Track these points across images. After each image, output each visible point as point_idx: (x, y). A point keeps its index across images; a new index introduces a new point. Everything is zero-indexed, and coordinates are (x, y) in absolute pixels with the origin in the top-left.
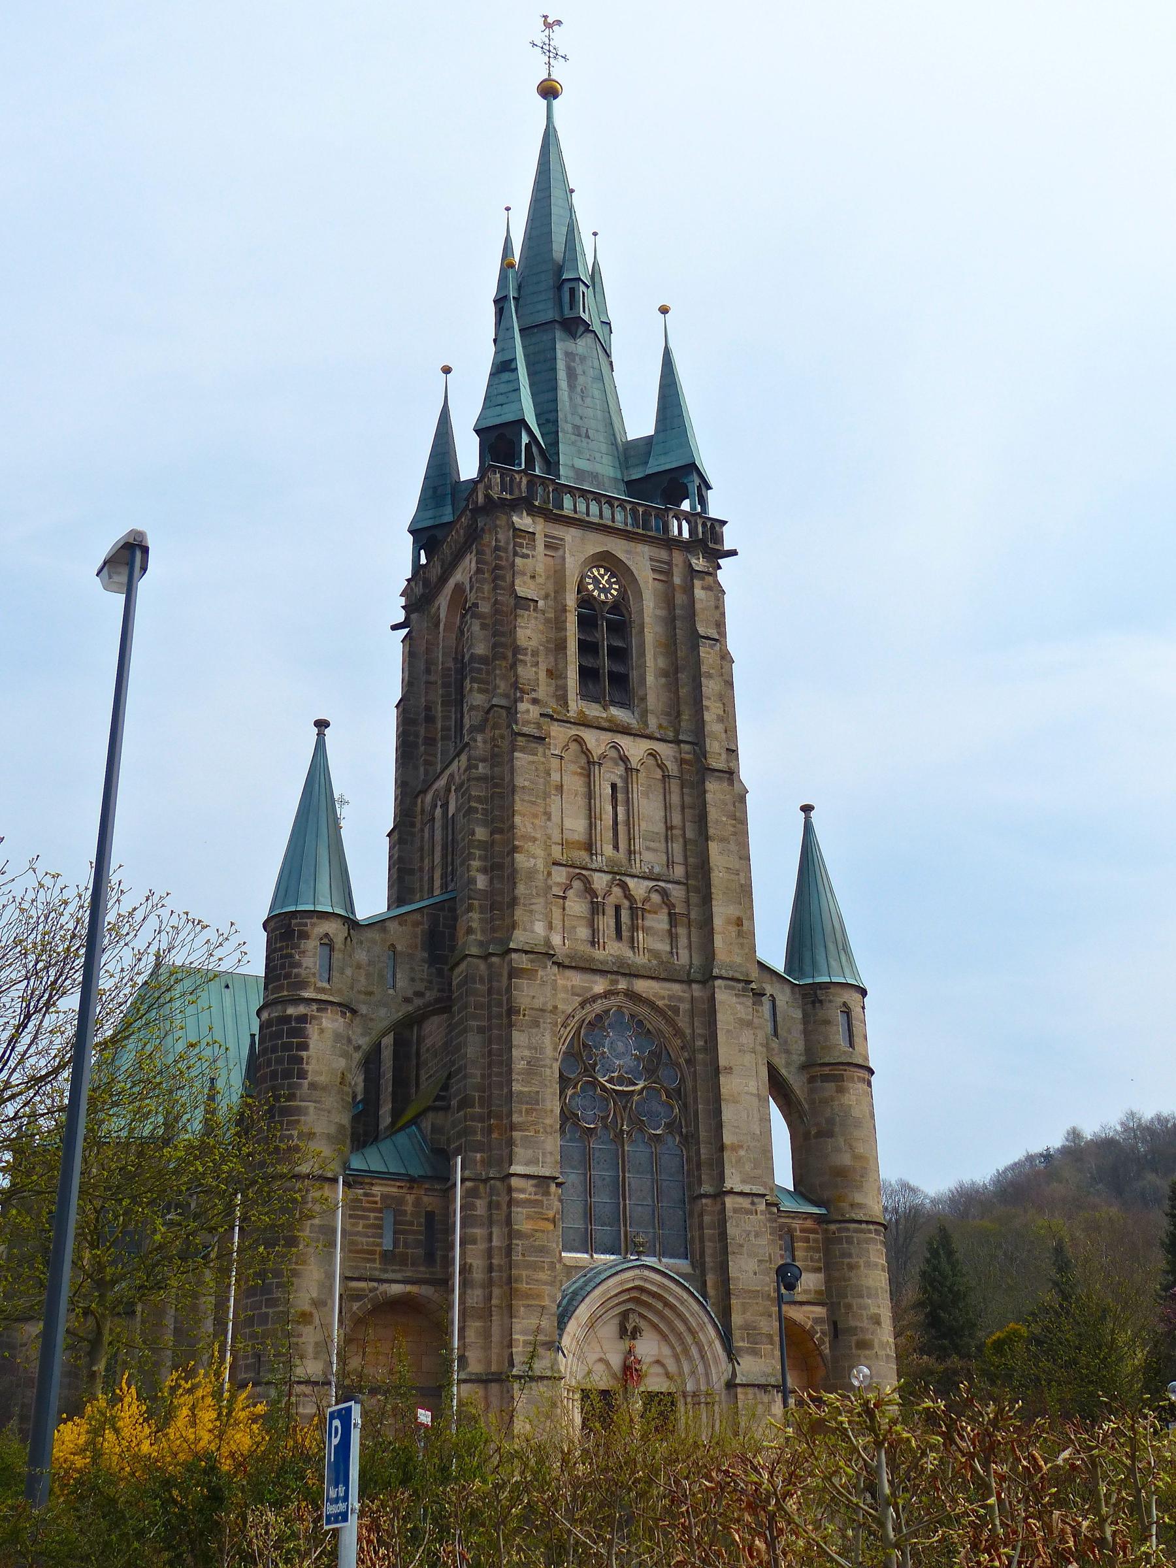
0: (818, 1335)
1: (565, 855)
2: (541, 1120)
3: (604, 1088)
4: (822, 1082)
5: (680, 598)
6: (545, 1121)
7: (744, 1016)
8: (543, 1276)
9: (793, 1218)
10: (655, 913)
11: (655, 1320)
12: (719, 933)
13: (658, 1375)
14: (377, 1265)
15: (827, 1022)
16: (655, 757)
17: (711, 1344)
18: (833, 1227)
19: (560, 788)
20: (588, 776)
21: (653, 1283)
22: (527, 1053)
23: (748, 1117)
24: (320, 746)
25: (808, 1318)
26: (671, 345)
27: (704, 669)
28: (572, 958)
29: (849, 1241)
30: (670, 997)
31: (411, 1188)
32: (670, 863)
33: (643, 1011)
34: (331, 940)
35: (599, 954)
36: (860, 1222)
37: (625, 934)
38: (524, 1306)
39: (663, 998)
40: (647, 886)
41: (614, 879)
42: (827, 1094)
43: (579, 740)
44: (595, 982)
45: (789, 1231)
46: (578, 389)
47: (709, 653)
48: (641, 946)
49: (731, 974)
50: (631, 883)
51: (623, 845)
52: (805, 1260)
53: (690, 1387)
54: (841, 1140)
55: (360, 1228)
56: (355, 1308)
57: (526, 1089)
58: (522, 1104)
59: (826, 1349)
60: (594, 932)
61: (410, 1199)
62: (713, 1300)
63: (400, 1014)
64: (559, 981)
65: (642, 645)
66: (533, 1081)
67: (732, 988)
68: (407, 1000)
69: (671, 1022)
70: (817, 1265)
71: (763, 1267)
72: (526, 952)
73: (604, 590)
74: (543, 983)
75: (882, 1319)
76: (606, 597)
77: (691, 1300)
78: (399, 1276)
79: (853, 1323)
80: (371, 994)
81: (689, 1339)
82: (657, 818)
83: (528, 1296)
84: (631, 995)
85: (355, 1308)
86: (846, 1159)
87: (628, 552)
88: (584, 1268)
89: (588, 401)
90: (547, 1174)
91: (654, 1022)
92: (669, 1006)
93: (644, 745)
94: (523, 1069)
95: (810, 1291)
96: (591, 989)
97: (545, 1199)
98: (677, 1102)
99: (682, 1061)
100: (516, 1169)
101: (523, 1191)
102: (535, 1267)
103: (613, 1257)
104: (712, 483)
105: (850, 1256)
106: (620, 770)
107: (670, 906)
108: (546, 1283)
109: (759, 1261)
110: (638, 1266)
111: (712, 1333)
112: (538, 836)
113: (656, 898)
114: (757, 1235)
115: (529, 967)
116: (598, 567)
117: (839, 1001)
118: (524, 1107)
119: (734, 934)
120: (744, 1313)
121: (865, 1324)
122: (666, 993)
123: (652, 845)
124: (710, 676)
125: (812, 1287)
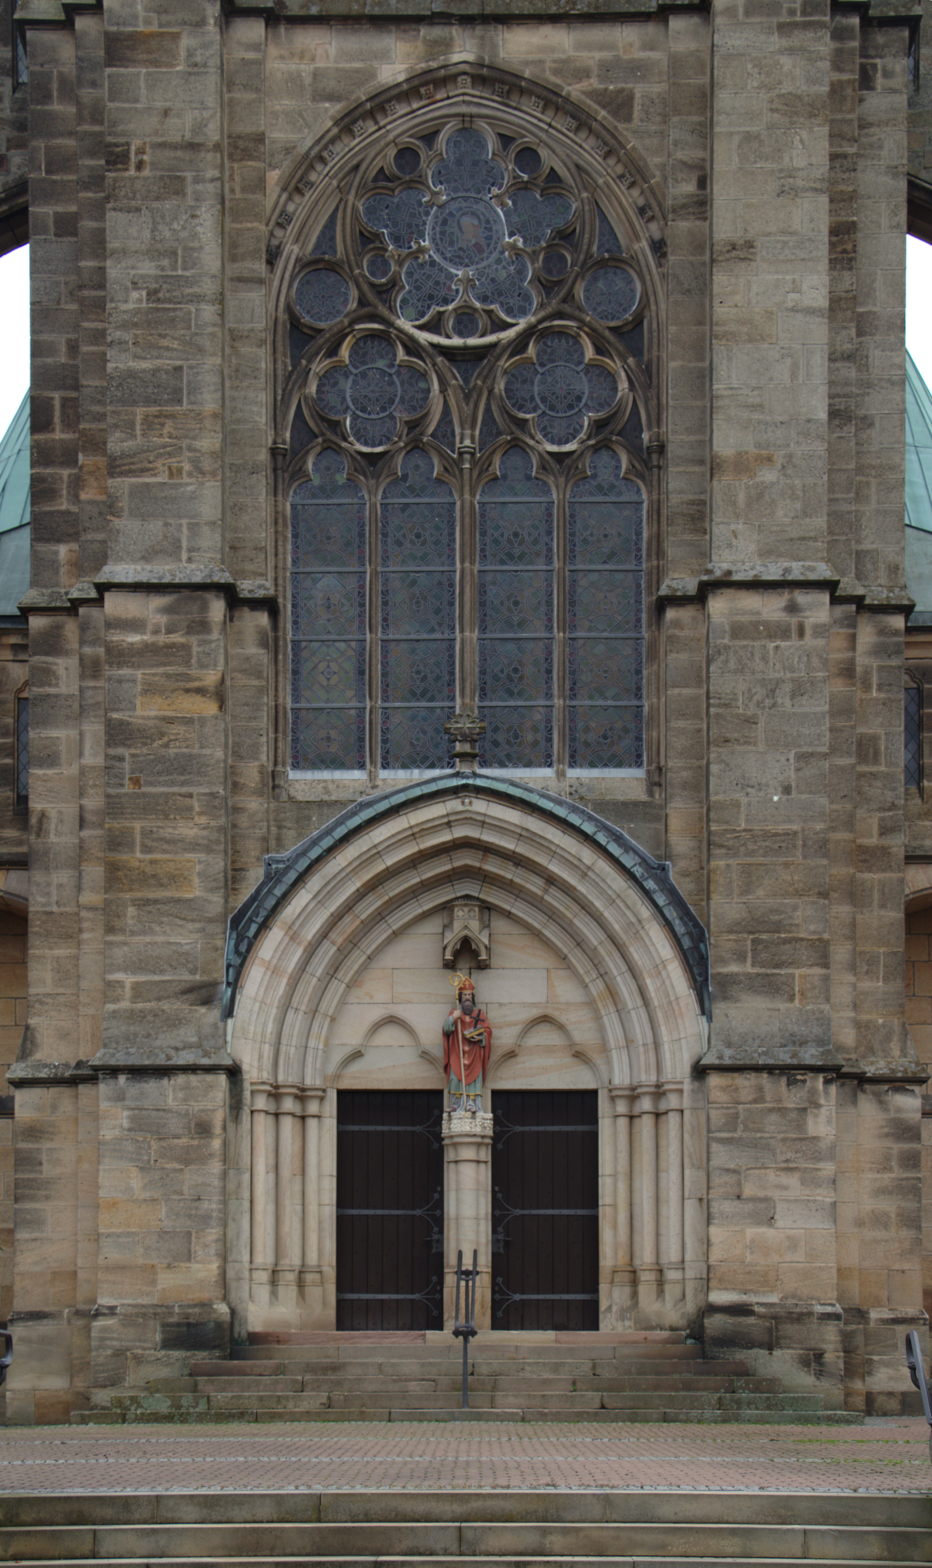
2: (185, 443)
3: (413, 347)
6: (197, 444)
7: (802, 88)
13: (549, 1050)
17: (659, 968)
21: (500, 828)
22: (147, 268)
23: (794, 376)
30: (607, 69)
38: (134, 902)
57: (145, 365)
58: (134, 403)
62: (682, 864)
66: (165, 342)
77: (603, 866)
81: (614, 964)
83: (146, 879)
90: (197, 578)
92: (601, 97)
94: (137, 311)
96: (371, 75)
97: (193, 640)
98: (624, 361)
109: (801, 757)
114: (796, 693)
115: (154, 28)
118: (140, 412)
120: (746, 890)
122: (592, 58)
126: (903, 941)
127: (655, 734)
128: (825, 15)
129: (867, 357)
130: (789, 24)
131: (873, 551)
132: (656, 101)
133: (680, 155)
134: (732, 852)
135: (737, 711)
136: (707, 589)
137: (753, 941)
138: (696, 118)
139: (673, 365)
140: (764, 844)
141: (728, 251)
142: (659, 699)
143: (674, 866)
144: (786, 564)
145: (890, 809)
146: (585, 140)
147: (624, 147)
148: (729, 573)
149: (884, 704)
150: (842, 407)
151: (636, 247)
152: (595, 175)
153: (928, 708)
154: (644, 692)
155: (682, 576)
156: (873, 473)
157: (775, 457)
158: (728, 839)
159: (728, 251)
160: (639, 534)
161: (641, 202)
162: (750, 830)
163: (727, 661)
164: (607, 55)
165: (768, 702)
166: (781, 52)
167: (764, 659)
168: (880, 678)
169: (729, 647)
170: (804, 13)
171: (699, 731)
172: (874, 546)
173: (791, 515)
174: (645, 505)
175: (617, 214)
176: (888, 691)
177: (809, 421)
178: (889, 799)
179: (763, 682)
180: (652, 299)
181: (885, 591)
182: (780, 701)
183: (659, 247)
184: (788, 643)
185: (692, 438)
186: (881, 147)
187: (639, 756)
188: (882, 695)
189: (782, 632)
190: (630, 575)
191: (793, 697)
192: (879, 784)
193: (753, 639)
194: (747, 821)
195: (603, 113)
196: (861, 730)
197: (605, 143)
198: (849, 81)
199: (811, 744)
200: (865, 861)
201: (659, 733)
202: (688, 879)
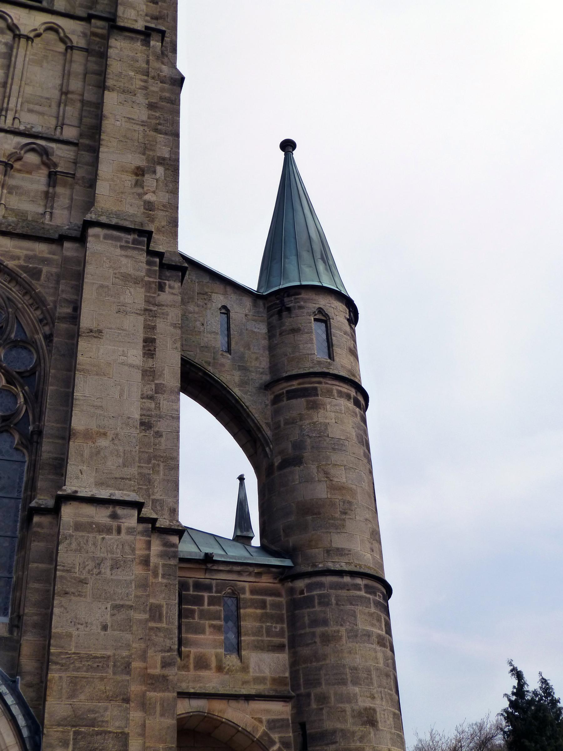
4: (289, 399)
9: (239, 573)
10: (29, 172)
16: (57, 31)
18: (301, 584)
23: (121, 395)
25: (260, 721)
29: (324, 601)
30: (28, 258)
36: (340, 573)
39: (18, 258)
40: (18, 143)
42: (294, 414)
45: (233, 593)
49: (114, 221)
52: (258, 632)
54: (313, 468)
62: (28, 678)
67: (118, 239)
69: (27, 290)
70: (277, 640)
71: (121, 616)
75: (379, 716)
79: (328, 725)
92: (25, 269)
98: (22, 388)
99: (40, 337)
105: (325, 623)
109: (115, 607)
114: (115, 566)
117: (313, 307)
119: (128, 184)
120: (72, 695)
121: (350, 725)
123: (37, 108)
126: (176, 739)
127: (18, 594)
128: (144, 246)
129: (159, 403)
130: (126, 246)
131: (161, 500)
132: (54, 275)
133: (64, 296)
134: (64, 667)
135: (74, 575)
136: (62, 500)
137: (75, 732)
138: (73, 282)
139: (51, 388)
140: (87, 663)
141: (88, 333)
142: (23, 573)
143: (22, 679)
144: (113, 491)
145: (168, 651)
146: (14, 287)
147: (34, 291)
148: (76, 492)
149: (166, 586)
150: (147, 421)
151: (36, 336)
152: (17, 303)
153: (184, 605)
154: (14, 569)
155: (46, 498)
156: (162, 459)
157: (108, 434)
158: (62, 659)
159: (88, 333)
160: (21, 479)
161: (41, 317)
162: (78, 653)
163: (71, 544)
164: (31, 253)
165: (95, 571)
166: (121, 256)
167: (94, 544)
168: (163, 570)
169: (73, 536)
170: (133, 243)
171: (48, 591)
172: (162, 497)
173: (116, 465)
174: (26, 464)
175: (27, 321)
176: (168, 579)
177: (129, 418)
178: (168, 645)
179: (93, 559)
180: (42, 361)
181: (168, 521)
182: (103, 570)
183: (49, 338)
184: (110, 537)
185: (59, 425)
186: (168, 315)
187: (6, 609)
188: (165, 581)
189: (109, 530)
190: (13, 501)
191: (112, 569)
192: (162, 635)
193: (89, 532)
194: (76, 647)
195: (25, 275)
196: (152, 600)
197: (24, 288)
198: (153, 282)
199: (122, 599)
200: (152, 684)
201: (21, 593)
202: (31, 689)
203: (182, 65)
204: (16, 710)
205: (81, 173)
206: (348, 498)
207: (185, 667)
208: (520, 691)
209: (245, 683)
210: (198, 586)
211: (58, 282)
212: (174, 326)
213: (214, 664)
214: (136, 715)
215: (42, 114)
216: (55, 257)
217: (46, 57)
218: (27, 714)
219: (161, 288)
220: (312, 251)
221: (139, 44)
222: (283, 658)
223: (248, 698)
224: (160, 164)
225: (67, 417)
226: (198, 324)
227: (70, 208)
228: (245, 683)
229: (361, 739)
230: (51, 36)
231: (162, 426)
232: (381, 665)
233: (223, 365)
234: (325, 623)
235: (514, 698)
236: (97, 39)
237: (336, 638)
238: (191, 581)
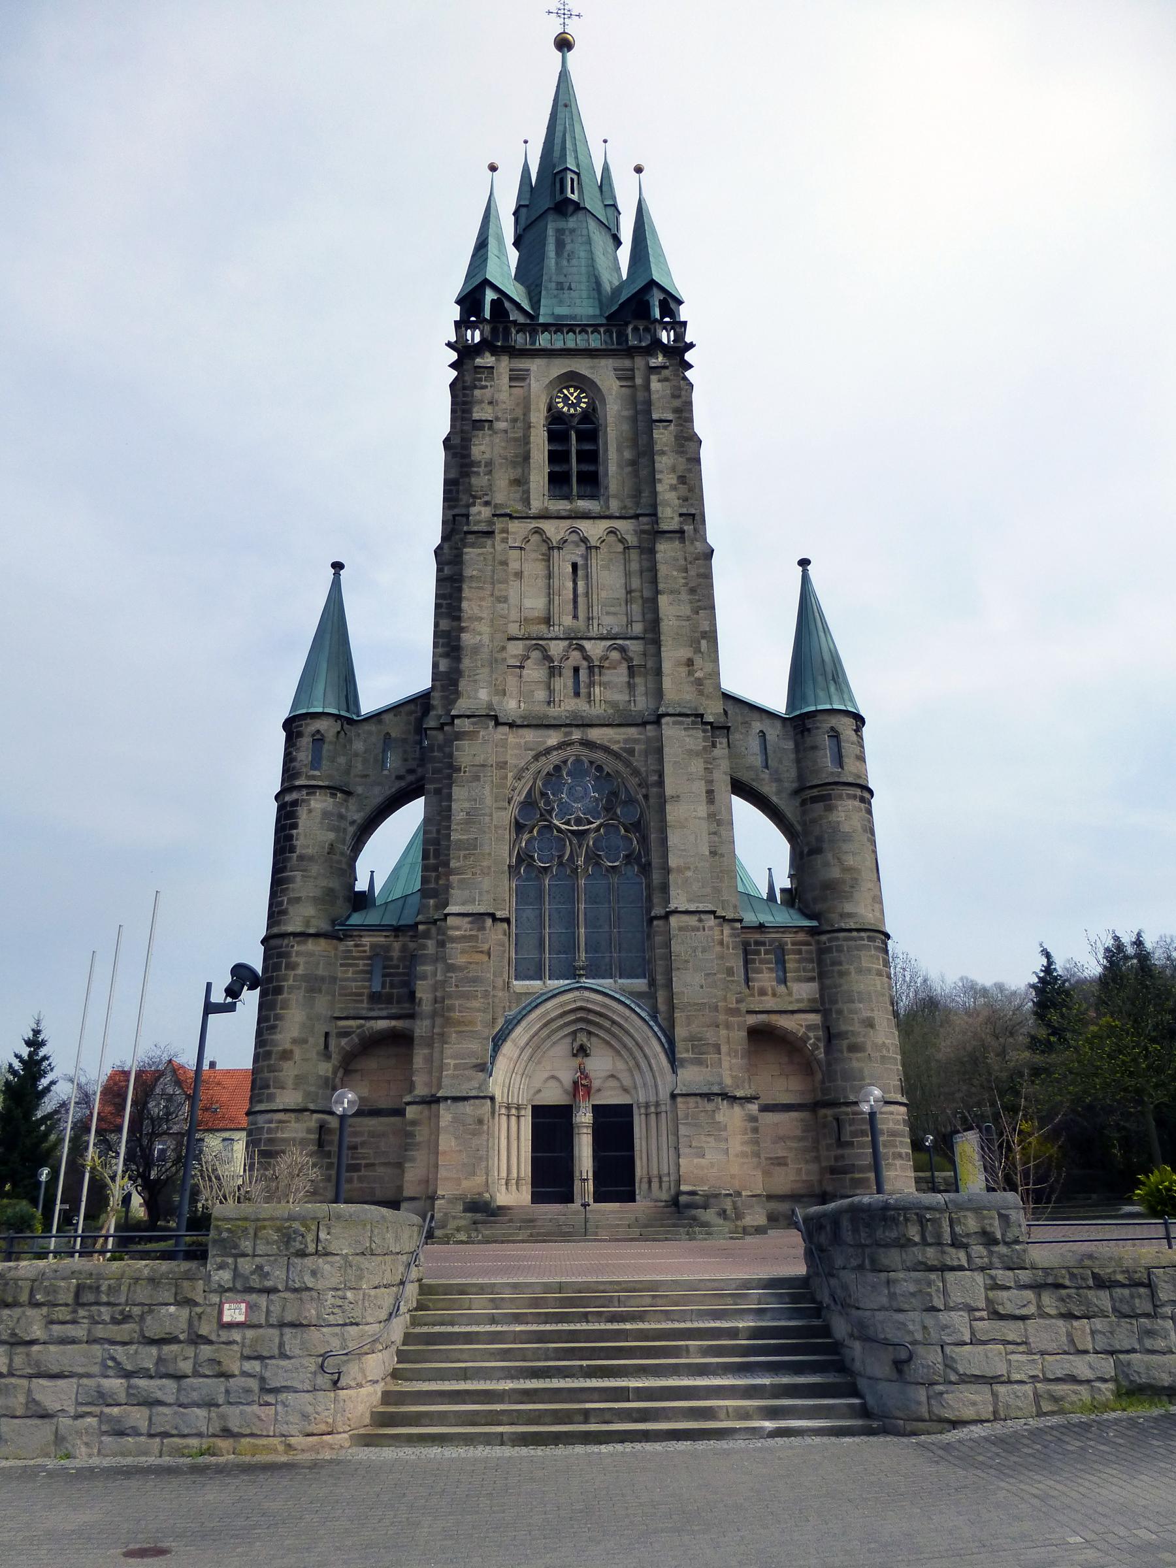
0: (811, 1041)
1: (523, 631)
3: (559, 830)
5: (641, 396)
8: (475, 1004)
9: (783, 932)
10: (615, 668)
11: (607, 1037)
12: (668, 675)
14: (365, 1005)
15: (814, 748)
18: (824, 938)
19: (519, 575)
20: (548, 559)
23: (696, 840)
24: (336, 585)
25: (802, 1026)
26: (645, 195)
27: (657, 448)
28: (524, 718)
29: (840, 949)
30: (626, 741)
31: (396, 936)
32: (630, 623)
33: (599, 756)
34: (322, 735)
35: (553, 711)
36: (850, 930)
37: (583, 691)
38: (456, 1032)
39: (619, 742)
41: (570, 645)
43: (538, 531)
44: (549, 737)
45: (780, 945)
46: (565, 255)
47: (662, 434)
48: (597, 699)
49: (678, 710)
50: (588, 645)
51: (582, 614)
52: (797, 970)
53: (642, 1099)
54: (830, 856)
55: (350, 975)
56: (343, 1043)
58: (460, 850)
59: (821, 1054)
60: (550, 690)
61: (397, 945)
63: (394, 790)
64: (509, 740)
65: (606, 443)
67: (681, 723)
68: (399, 778)
69: (628, 764)
72: (469, 717)
73: (573, 405)
74: (485, 742)
75: (877, 1021)
76: (576, 410)
78: (384, 1013)
79: (844, 1028)
80: (366, 776)
82: (618, 586)
83: (459, 1023)
84: (587, 744)
85: (343, 1043)
86: (835, 873)
87: (592, 368)
88: (535, 993)
89: (574, 262)
90: (482, 911)
91: (610, 765)
92: (625, 750)
93: (604, 525)
94: (461, 820)
95: (803, 999)
97: (480, 934)
99: (640, 797)
100: (452, 909)
101: (458, 928)
102: (467, 996)
103: (562, 982)
104: (682, 293)
106: (582, 550)
107: (629, 660)
108: (479, 1010)
110: (577, 988)
111: (658, 1049)
112: (484, 615)
113: (615, 655)
116: (567, 388)
118: (462, 853)
119: (683, 675)
120: (688, 1025)
123: (612, 609)
124: (663, 453)
125: (805, 996)
133: (652, 768)
134: (682, 1010)
179: (691, 947)
183: (646, 797)
189: (698, 930)
203: (711, 539)
204: (659, 1034)
205: (650, 664)
206: (855, 876)
207: (753, 995)
208: (1048, 970)
209: (791, 1003)
210: (757, 943)
211: (646, 757)
212: (725, 773)
213: (770, 992)
214: (723, 1032)
215: (615, 614)
216: (642, 737)
217: (611, 560)
218: (665, 1035)
219: (714, 745)
220: (825, 674)
221: (677, 543)
222: (814, 986)
223: (793, 1012)
224: (703, 638)
225: (665, 856)
226: (743, 749)
227: (646, 694)
228: (791, 1003)
229: (864, 1036)
230: (612, 538)
231: (723, 850)
232: (879, 989)
233: (763, 780)
234: (840, 964)
235: (1042, 974)
236: (645, 536)
237: (847, 973)
238: (752, 940)
